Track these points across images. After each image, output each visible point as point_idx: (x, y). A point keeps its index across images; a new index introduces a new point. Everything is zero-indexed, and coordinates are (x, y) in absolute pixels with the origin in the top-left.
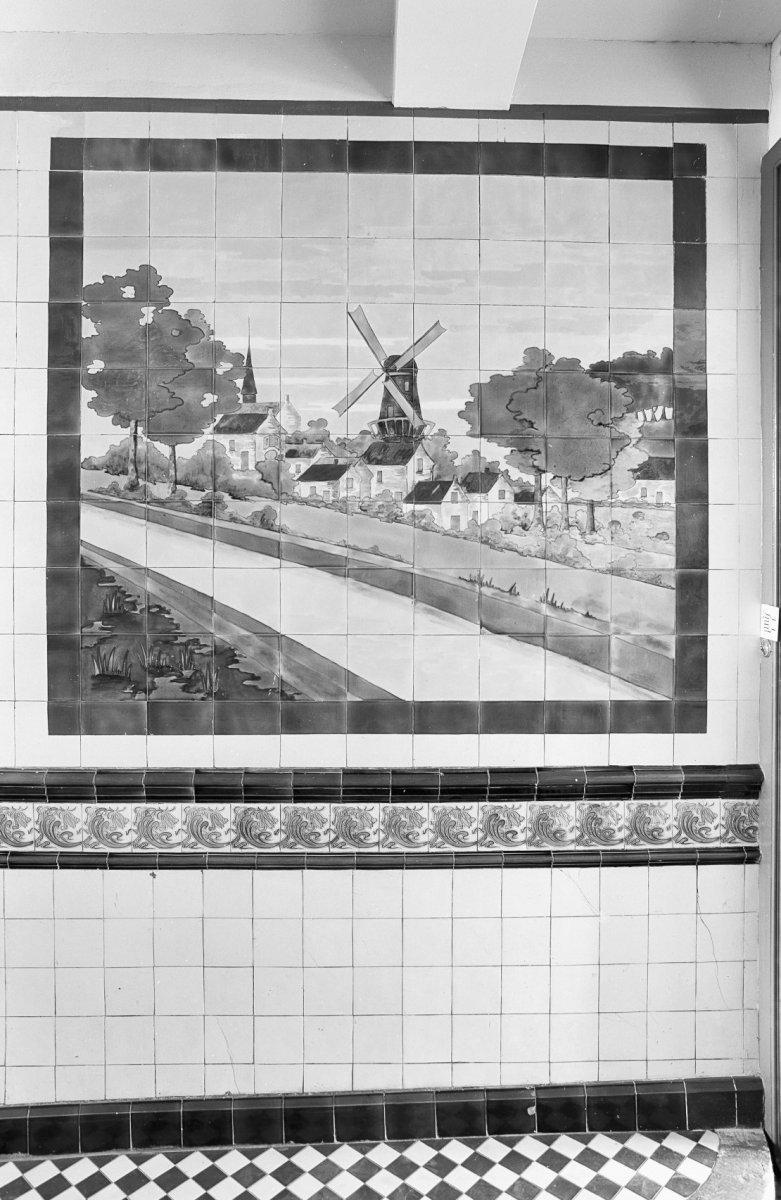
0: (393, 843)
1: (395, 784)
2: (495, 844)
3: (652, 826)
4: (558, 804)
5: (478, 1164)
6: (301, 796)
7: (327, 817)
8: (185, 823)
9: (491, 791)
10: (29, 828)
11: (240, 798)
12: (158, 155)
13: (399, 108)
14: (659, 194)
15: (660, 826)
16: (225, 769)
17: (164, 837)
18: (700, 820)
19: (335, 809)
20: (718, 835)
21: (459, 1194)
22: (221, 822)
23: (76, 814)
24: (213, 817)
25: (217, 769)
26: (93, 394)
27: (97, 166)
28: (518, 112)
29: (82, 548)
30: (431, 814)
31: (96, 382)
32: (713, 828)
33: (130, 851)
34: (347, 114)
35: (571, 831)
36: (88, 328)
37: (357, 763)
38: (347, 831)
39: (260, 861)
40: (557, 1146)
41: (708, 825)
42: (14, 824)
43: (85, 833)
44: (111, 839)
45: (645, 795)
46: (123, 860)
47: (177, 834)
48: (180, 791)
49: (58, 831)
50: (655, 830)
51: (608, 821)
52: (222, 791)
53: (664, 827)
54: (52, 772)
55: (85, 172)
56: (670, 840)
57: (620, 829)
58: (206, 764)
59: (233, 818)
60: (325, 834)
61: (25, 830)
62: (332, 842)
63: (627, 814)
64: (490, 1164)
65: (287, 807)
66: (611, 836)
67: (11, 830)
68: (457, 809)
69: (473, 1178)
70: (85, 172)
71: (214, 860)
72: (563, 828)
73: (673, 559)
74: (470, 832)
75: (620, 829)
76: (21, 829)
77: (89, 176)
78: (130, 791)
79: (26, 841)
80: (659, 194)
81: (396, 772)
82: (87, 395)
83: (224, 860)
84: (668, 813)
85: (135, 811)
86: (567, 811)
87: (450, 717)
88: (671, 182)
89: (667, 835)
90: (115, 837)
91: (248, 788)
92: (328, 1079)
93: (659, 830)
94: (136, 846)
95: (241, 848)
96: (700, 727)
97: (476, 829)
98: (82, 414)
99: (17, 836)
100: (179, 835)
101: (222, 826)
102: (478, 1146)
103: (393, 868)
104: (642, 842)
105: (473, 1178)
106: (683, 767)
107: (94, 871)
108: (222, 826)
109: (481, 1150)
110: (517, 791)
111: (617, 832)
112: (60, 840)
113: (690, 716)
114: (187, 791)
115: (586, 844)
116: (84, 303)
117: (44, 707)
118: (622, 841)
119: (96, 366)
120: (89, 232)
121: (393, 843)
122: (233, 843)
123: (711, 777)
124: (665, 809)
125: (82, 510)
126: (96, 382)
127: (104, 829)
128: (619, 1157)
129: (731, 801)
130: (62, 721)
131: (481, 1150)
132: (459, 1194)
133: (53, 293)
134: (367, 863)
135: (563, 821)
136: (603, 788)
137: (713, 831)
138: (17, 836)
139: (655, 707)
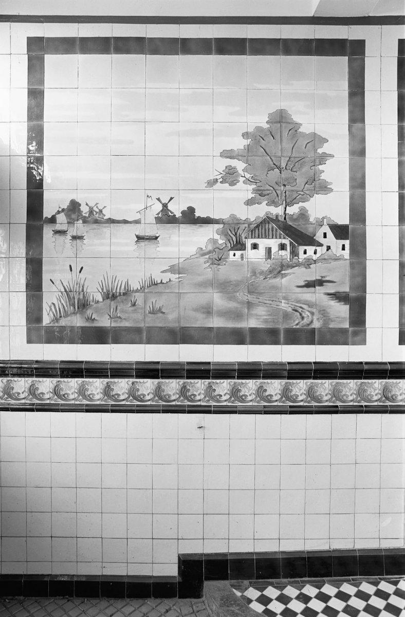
0: (209, 401)
2: (211, 402)
5: (284, 599)
6: (63, 375)
10: (199, 392)
14: (50, 60)
16: (48, 361)
21: (277, 614)
33: (124, 403)
38: (32, 391)
40: (305, 591)
43: (126, 394)
45: (350, 377)
46: (121, 408)
47: (23, 393)
48: (102, 372)
51: (395, 391)
52: (96, 372)
56: (277, 401)
62: (379, 400)
64: (270, 600)
65: (333, 382)
69: (282, 607)
72: (397, 393)
75: (301, 395)
79: (197, 399)
80: (50, 60)
81: (87, 362)
83: (322, 409)
85: (203, 384)
86: (399, 384)
88: (45, 55)
89: (249, 398)
91: (63, 370)
92: (242, 545)
93: (396, 396)
94: (255, 402)
95: (5, 400)
96: (363, 342)
102: (264, 590)
103: (120, 412)
105: (282, 607)
106: (389, 362)
107: (168, 414)
108: (70, 390)
109: (265, 593)
111: (350, 396)
112: (190, 399)
115: (182, 401)
118: (327, 401)
121: (209, 401)
123: (377, 367)
131: (265, 593)
132: (277, 614)
137: (21, 394)
139: (39, 319)
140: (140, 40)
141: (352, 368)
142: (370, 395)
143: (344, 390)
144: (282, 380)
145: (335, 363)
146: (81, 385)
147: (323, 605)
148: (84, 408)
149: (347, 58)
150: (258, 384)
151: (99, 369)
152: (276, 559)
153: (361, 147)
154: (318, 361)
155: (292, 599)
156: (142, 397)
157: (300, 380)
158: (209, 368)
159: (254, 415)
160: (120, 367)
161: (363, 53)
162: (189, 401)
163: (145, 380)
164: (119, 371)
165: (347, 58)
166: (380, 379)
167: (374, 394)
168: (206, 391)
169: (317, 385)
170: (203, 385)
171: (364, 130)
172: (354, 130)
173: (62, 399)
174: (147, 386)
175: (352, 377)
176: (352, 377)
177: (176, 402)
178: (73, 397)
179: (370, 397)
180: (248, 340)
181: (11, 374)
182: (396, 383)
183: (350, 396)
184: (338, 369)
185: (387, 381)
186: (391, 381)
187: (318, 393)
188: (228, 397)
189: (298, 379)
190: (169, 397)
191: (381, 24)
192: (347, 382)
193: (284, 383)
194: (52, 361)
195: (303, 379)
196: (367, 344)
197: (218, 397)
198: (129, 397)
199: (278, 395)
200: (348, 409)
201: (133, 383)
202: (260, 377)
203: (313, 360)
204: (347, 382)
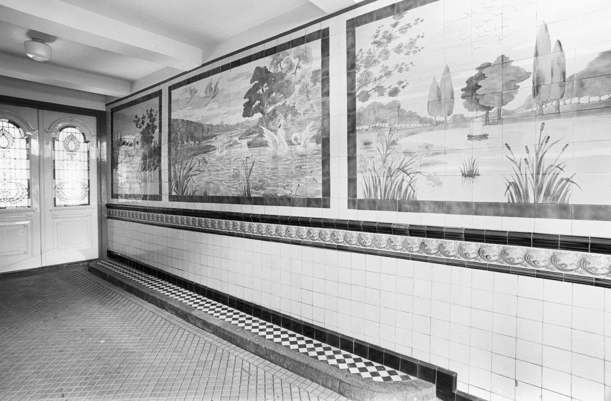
1: (465, 232)
9: (445, 235)
13: (354, 32)
19: (548, 251)
22: (327, 234)
28: (204, 65)
35: (434, 250)
39: (489, 267)
44: (411, 250)
48: (458, 236)
54: (337, 220)
57: (473, 254)
63: (436, 244)
71: (491, 267)
74: (599, 269)
75: (473, 254)
78: (458, 236)
84: (451, 245)
91: (324, 224)
101: (353, 238)
104: (504, 263)
110: (500, 239)
113: (324, 202)
115: (287, 237)
122: (418, 252)
123: (572, 240)
124: (472, 246)
128: (226, 318)
134: (340, 248)
136: (571, 244)
141: (369, 225)
147: (238, 321)
148: (536, 273)
150: (478, 245)
152: (326, 333)
154: (536, 232)
155: (347, 364)
158: (529, 237)
159: (543, 279)
162: (444, 255)
163: (492, 245)
164: (453, 235)
173: (531, 265)
174: (472, 247)
177: (574, 271)
178: (495, 259)
181: (560, 247)
188: (418, 249)
190: (513, 261)
200: (405, 256)
201: (528, 250)
203: (532, 231)
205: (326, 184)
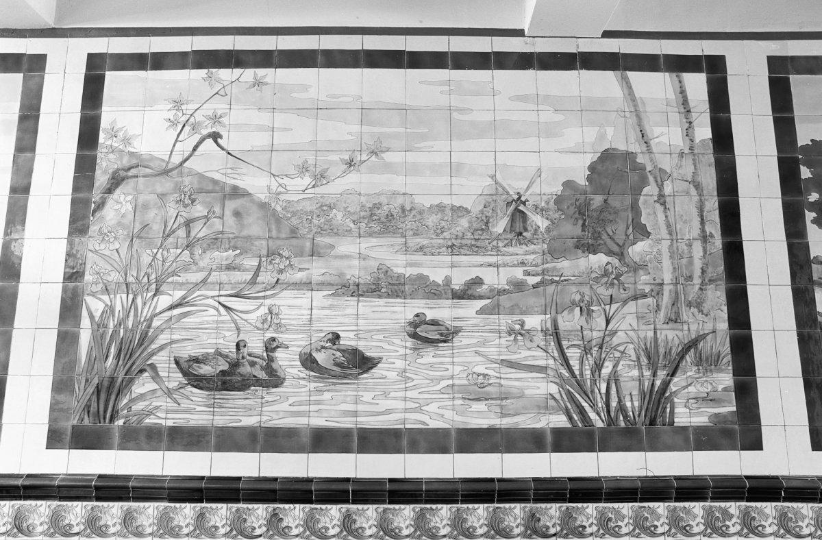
3: (358, 525)
4: (33, 503)
7: (662, 513)
8: (775, 518)
10: (661, 522)
11: (671, 499)
12: (139, 62)
15: (437, 525)
17: (397, 531)
18: (614, 520)
20: (772, 532)
23: (804, 511)
24: (795, 514)
25: (358, 479)
26: (814, 215)
27: (798, 73)
29: (819, 317)
30: (375, 513)
31: (813, 206)
32: (804, 526)
34: (701, 39)
35: (481, 527)
36: (805, 173)
37: (544, 473)
41: (620, 523)
42: (614, 520)
43: (301, 527)
49: (611, 524)
50: (68, 525)
53: (367, 526)
55: (790, 76)
58: (398, 475)
59: (737, 514)
60: (517, 527)
61: (803, 525)
66: (511, 531)
67: (612, 524)
68: (757, 507)
70: (790, 76)
73: (727, 324)
76: (800, 523)
77: (794, 79)
79: (256, 534)
82: (810, 216)
85: (450, 510)
86: (112, 510)
87: (435, 442)
90: (617, 529)
97: (226, 524)
98: (808, 227)
99: (798, 529)
100: (482, 529)
114: (670, 493)
116: (800, 157)
117: (807, 429)
119: (814, 197)
120: (798, 112)
125: (816, 292)
126: (813, 206)
127: (752, 522)
129: (418, 506)
130: (55, 439)
133: (779, 150)
135: (73, 518)
138: (798, 529)
140: (313, 53)
142: (435, 527)
143: (177, 519)
144: (416, 505)
145: (127, 478)
146: (419, 514)
149: (21, 75)
151: (512, 490)
153: (172, 185)
156: (397, 531)
157: (332, 506)
160: (368, 487)
161: (42, 69)
165: (21, 75)
166: (12, 500)
167: (514, 525)
168: (561, 518)
169: (357, 512)
170: (156, 511)
171: (32, 160)
172: (20, 161)
175: (362, 500)
176: (362, 500)
179: (434, 531)
180: (549, 447)
182: (400, 509)
183: (39, 527)
184: (422, 491)
185: (22, 502)
186: (28, 503)
187: (469, 524)
189: (763, 501)
191: (492, 36)
192: (510, 507)
193: (455, 509)
194: (516, 478)
195: (771, 501)
196: (815, 452)
197: (581, 529)
198: (816, 531)
199: (665, 525)
202: (816, 499)
204: (510, 507)
205: (746, 390)
